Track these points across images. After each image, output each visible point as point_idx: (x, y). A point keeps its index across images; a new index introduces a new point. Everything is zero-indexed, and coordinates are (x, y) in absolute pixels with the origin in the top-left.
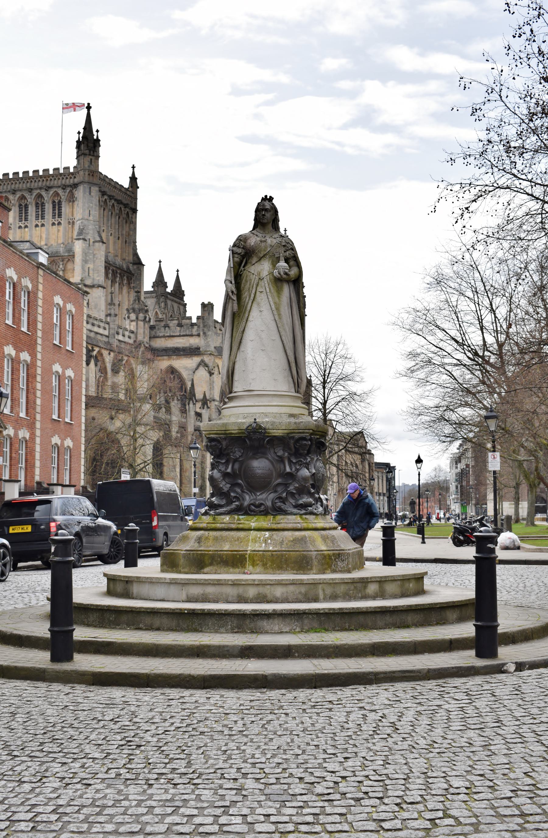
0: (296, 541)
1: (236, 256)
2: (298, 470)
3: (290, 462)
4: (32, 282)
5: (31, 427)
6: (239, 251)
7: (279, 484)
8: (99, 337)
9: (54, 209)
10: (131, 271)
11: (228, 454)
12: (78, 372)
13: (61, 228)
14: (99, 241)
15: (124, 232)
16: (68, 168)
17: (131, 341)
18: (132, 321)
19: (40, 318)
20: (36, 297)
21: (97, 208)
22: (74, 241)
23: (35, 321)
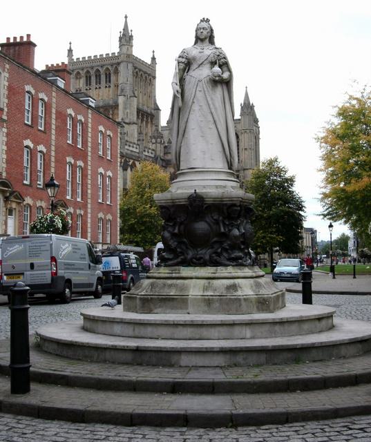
0: (229, 288)
2: (230, 231)
3: (224, 224)
4: (84, 117)
5: (84, 206)
6: (184, 60)
7: (216, 242)
9: (106, 79)
11: (175, 219)
12: (115, 174)
16: (114, 53)
17: (153, 156)
18: (153, 143)
19: (90, 140)
20: (87, 127)
23: (87, 141)
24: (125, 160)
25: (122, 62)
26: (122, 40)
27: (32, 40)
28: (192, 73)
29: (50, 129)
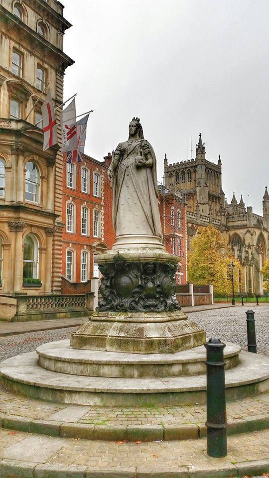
1: (116, 155)
3: (141, 278)
6: (118, 152)
8: (205, 223)
13: (191, 183)
25: (198, 165)
26: (199, 151)
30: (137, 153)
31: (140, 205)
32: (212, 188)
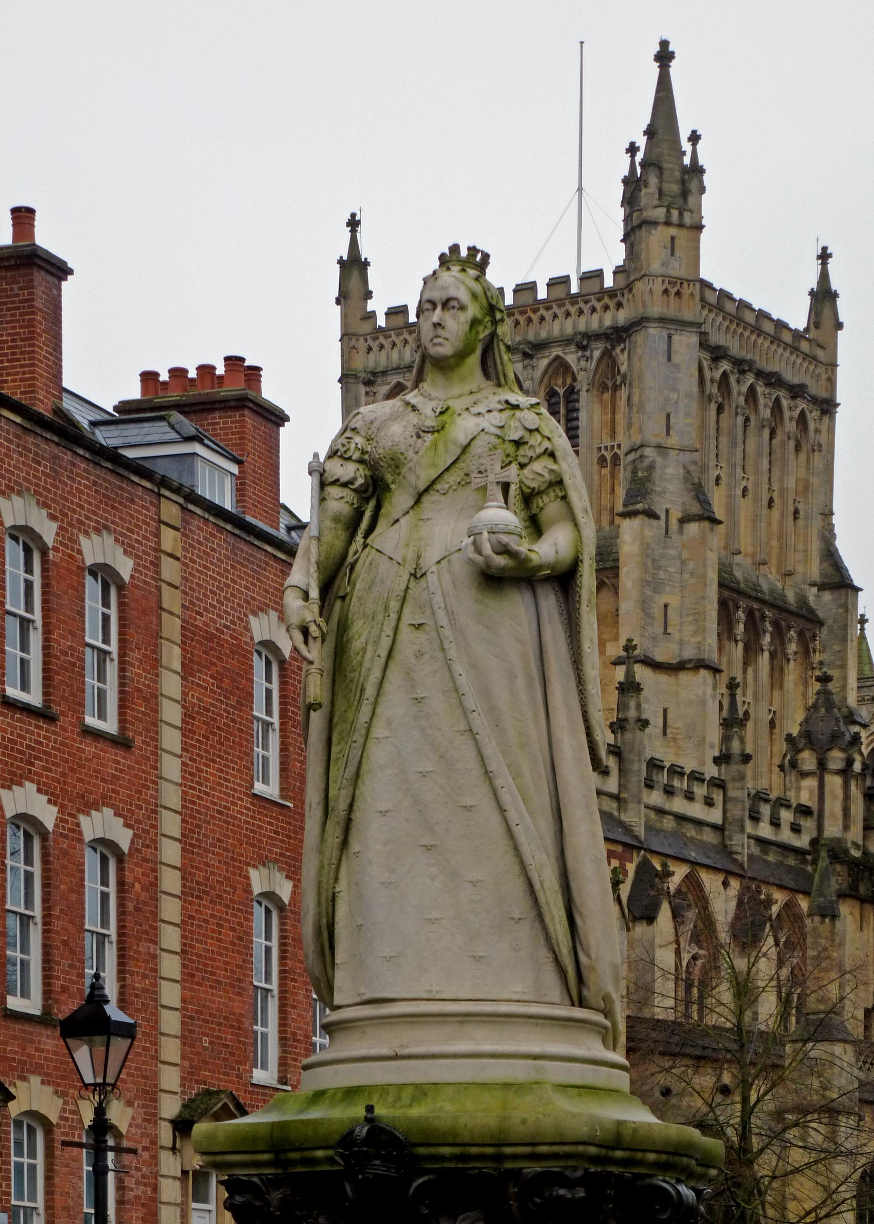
1: (334, 492)
6: (347, 471)
8: (691, 831)
10: (811, 611)
14: (699, 518)
15: (791, 483)
16: (598, 274)
18: (804, 775)
21: (694, 405)
22: (618, 520)
24: (644, 868)
26: (648, 195)
27: (46, 237)
28: (387, 537)
29: (153, 724)
30: (484, 489)
31: (495, 820)
32: (749, 536)
